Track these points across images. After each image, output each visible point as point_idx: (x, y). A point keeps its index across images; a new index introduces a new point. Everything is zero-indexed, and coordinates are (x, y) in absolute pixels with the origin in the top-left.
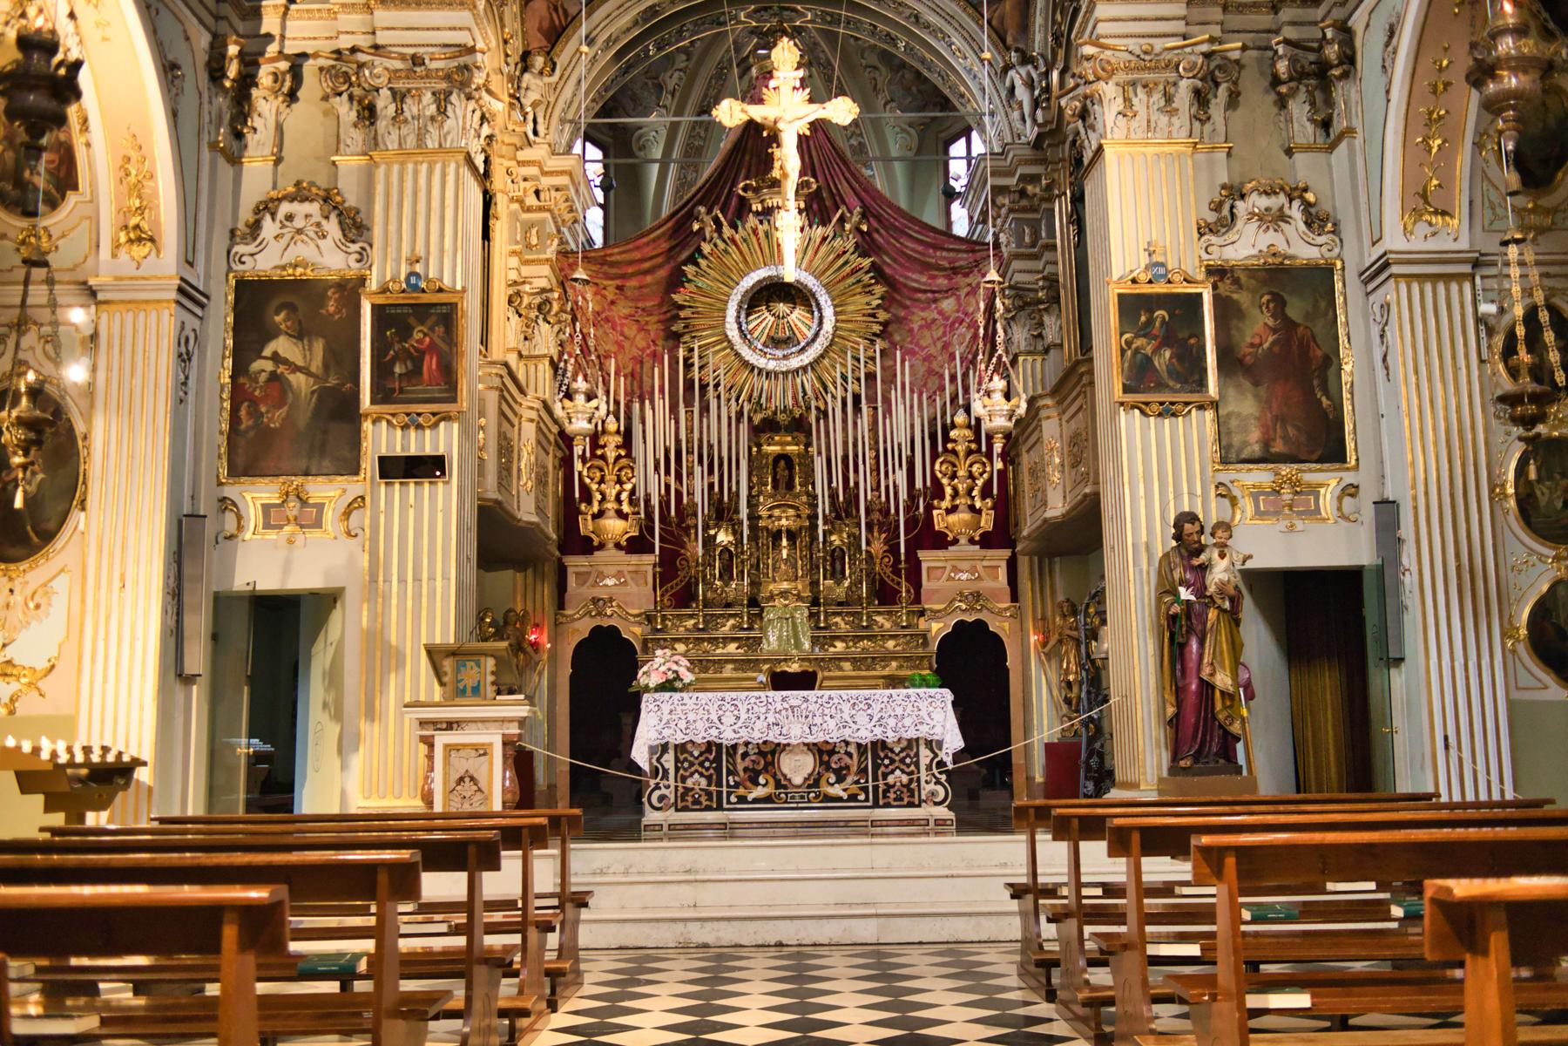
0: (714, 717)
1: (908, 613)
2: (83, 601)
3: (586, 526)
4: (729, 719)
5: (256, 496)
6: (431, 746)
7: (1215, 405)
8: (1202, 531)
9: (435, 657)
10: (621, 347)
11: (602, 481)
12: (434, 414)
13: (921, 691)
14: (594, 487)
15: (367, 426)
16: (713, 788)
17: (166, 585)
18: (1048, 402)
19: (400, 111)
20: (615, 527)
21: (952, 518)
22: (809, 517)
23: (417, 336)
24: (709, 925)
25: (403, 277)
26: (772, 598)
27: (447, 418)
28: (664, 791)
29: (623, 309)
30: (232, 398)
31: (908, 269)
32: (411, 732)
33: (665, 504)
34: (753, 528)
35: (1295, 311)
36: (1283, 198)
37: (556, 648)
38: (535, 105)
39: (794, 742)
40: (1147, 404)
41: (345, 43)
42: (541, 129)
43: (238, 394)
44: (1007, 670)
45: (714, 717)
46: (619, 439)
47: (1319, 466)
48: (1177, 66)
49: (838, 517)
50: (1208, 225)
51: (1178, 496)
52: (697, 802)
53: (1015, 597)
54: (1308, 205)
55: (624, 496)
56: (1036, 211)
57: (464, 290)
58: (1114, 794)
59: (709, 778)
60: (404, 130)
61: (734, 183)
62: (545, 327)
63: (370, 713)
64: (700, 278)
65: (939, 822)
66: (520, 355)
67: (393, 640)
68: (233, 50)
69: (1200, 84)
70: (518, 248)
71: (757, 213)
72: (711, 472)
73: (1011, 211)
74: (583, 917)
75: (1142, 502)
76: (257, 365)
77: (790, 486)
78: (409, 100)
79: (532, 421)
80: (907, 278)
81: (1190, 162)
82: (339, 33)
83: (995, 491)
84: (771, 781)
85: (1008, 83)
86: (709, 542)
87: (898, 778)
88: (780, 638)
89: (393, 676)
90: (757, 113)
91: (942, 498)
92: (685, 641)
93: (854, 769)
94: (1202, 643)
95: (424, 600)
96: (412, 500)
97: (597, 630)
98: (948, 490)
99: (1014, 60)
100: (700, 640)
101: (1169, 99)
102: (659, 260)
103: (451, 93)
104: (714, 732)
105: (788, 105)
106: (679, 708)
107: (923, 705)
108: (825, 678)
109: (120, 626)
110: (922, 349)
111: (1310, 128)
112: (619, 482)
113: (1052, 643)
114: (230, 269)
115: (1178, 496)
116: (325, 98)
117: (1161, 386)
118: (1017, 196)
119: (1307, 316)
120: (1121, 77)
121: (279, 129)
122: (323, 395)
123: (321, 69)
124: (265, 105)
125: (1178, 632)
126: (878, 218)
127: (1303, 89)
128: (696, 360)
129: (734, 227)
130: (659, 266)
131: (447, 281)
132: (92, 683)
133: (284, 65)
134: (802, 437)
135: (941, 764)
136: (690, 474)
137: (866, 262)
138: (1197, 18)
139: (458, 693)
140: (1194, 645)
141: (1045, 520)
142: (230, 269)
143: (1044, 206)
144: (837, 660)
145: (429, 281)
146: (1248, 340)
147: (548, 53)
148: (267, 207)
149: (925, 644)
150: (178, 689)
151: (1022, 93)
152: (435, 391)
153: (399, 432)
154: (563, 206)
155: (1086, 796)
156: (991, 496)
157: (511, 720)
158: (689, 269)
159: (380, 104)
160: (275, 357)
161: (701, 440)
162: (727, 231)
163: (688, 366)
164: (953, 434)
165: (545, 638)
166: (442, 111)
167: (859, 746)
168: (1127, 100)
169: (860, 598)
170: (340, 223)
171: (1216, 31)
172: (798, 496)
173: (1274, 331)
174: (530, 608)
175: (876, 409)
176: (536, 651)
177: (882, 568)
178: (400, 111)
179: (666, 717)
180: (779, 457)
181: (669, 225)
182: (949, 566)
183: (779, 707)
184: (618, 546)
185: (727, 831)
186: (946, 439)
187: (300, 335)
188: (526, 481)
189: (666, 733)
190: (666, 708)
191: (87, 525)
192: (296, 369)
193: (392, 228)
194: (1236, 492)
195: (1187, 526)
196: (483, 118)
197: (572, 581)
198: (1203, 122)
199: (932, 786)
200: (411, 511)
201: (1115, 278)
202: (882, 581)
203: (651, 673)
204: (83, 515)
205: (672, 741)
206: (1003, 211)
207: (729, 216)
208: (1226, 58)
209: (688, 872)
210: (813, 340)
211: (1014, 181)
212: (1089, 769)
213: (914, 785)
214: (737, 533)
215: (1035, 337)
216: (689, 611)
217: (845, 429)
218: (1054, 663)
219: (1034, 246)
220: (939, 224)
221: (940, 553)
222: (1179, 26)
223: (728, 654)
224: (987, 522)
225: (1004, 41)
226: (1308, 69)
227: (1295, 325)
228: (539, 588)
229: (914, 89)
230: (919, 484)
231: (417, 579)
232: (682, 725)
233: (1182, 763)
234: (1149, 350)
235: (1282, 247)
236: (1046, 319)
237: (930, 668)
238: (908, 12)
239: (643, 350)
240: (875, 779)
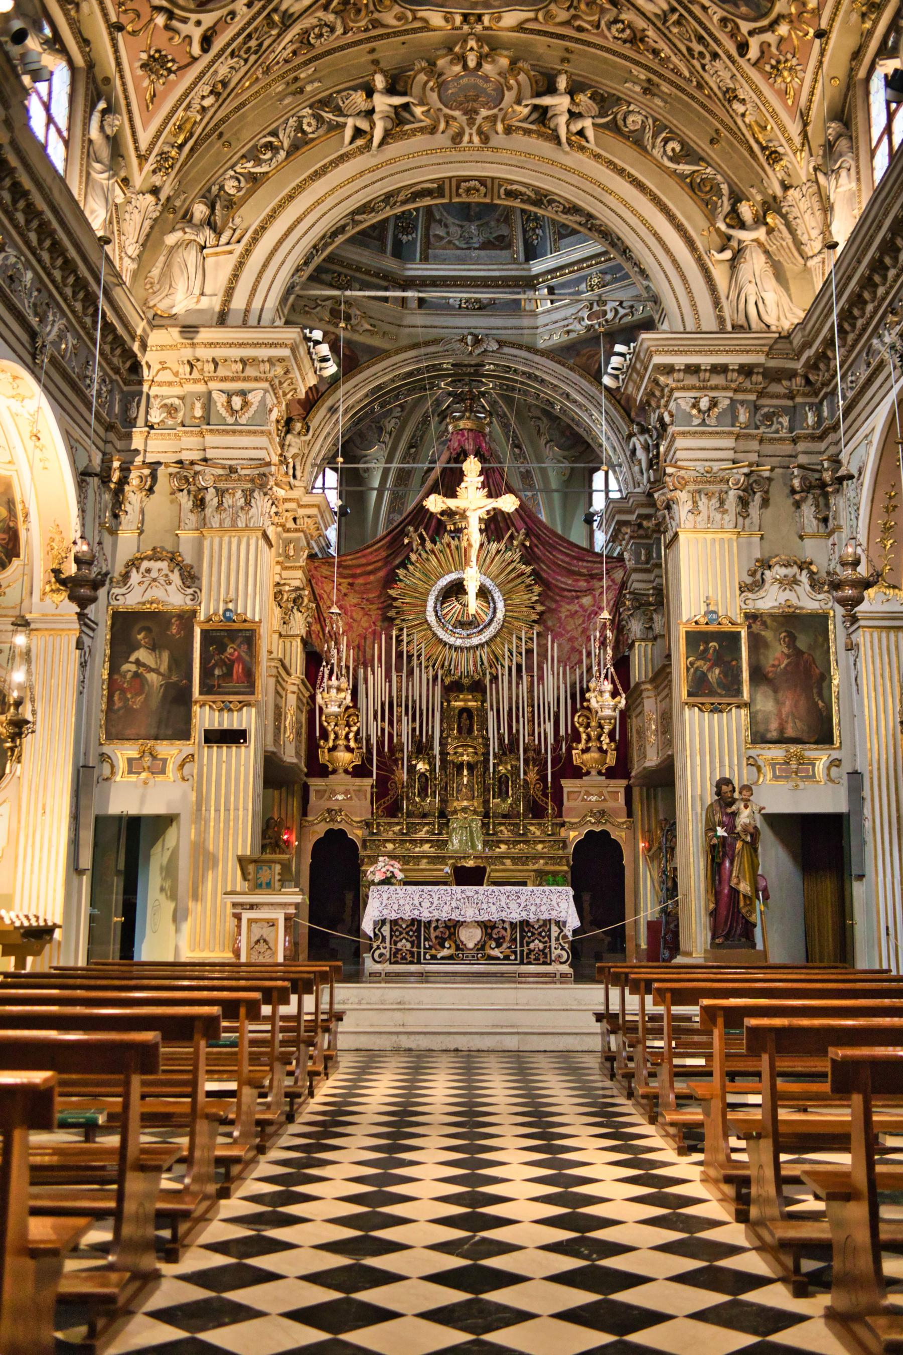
2: (19, 822)
3: (323, 757)
4: (426, 904)
5: (123, 753)
6: (240, 919)
7: (746, 705)
8: (734, 790)
9: (244, 864)
12: (240, 702)
13: (553, 888)
15: (196, 708)
16: (415, 949)
17: (71, 812)
18: (648, 686)
19: (220, 503)
20: (344, 757)
21: (586, 756)
22: (483, 754)
23: (230, 650)
24: (412, 1037)
25: (221, 612)
26: (455, 812)
27: (248, 704)
28: (382, 951)
29: (353, 599)
30: (109, 688)
31: (559, 574)
32: (230, 910)
33: (380, 743)
34: (443, 761)
35: (802, 643)
36: (795, 569)
37: (301, 845)
38: (294, 457)
39: (468, 920)
40: (703, 704)
41: (186, 456)
42: (298, 474)
43: (112, 686)
44: (622, 868)
47: (815, 746)
48: (728, 481)
49: (504, 754)
50: (746, 585)
51: (722, 765)
52: (404, 958)
53: (630, 814)
54: (812, 574)
55: (351, 735)
56: (649, 538)
57: (260, 621)
58: (679, 960)
59: (412, 943)
60: (224, 515)
62: (298, 615)
63: (196, 897)
64: (409, 577)
65: (563, 975)
66: (280, 635)
67: (211, 848)
68: (116, 464)
69: (741, 493)
70: (280, 559)
71: (451, 531)
72: (414, 720)
73: (631, 537)
74: (339, 1030)
75: (698, 768)
76: (125, 667)
77: (470, 731)
78: (227, 496)
80: (557, 580)
81: (735, 544)
82: (182, 449)
84: (453, 945)
85: (631, 446)
86: (412, 769)
87: (537, 945)
88: (460, 841)
89: (210, 872)
90: (452, 503)
91: (579, 741)
92: (393, 841)
93: (508, 939)
94: (732, 863)
95: (231, 823)
96: (224, 758)
97: (330, 832)
98: (584, 736)
99: (635, 430)
100: (403, 842)
101: (722, 502)
102: (380, 564)
103: (254, 491)
104: (416, 912)
105: (473, 500)
107: (554, 897)
108: (492, 871)
109: (42, 837)
111: (815, 522)
112: (348, 725)
113: (654, 849)
114: (109, 604)
115: (722, 765)
116: (173, 493)
117: (712, 693)
118: (636, 528)
119: (810, 647)
120: (691, 487)
121: (142, 512)
122: (168, 686)
123: (171, 474)
124: (133, 497)
125: (718, 854)
126: (538, 537)
127: (810, 496)
128: (405, 637)
129: (434, 542)
130: (379, 569)
131: (249, 615)
132: (24, 874)
133: (147, 472)
134: (479, 696)
135: (565, 937)
136: (399, 720)
137: (529, 569)
138: (742, 448)
139: (258, 886)
140: (727, 864)
141: (645, 768)
142: (109, 604)
143: (655, 536)
144: (501, 858)
145: (237, 615)
146: (771, 662)
147: (304, 419)
148: (134, 563)
150: (75, 877)
151: (641, 454)
152: (241, 687)
153: (217, 713)
154: (312, 527)
155: (664, 961)
157: (290, 904)
158: (401, 572)
159: (208, 498)
160: (138, 662)
161: (407, 697)
162: (429, 545)
163: (399, 642)
165: (294, 838)
166: (248, 503)
167: (511, 923)
168: (695, 502)
169: (519, 812)
170: (181, 575)
171: (754, 457)
172: (475, 739)
173: (788, 656)
174: (283, 816)
175: (532, 676)
176: (288, 847)
177: (535, 791)
178: (220, 503)
182: (583, 790)
184: (346, 771)
185: (424, 977)
187: (154, 648)
188: (289, 734)
189: (385, 912)
190: (385, 896)
191: (22, 773)
192: (150, 670)
193: (214, 579)
194: (761, 763)
195: (724, 788)
196: (273, 504)
198: (744, 518)
199: (559, 951)
200: (224, 765)
201: (684, 620)
202: (534, 800)
203: (376, 871)
204: (19, 766)
205: (389, 918)
206: (627, 537)
207: (430, 532)
208: (760, 476)
209: (399, 1003)
210: (489, 624)
211: (634, 517)
212: (666, 942)
213: (547, 950)
214: (431, 764)
216: (396, 820)
217: (510, 688)
218: (656, 863)
219: (647, 562)
220: (585, 544)
221: (577, 781)
222: (730, 454)
223: (423, 852)
224: (611, 759)
225: (629, 415)
226: (814, 483)
227: (803, 653)
228: (290, 800)
230: (562, 732)
231: (227, 810)
232: (396, 907)
233: (717, 941)
234: (705, 668)
235: (794, 601)
236: (655, 616)
237: (568, 865)
239: (366, 629)
240: (522, 945)
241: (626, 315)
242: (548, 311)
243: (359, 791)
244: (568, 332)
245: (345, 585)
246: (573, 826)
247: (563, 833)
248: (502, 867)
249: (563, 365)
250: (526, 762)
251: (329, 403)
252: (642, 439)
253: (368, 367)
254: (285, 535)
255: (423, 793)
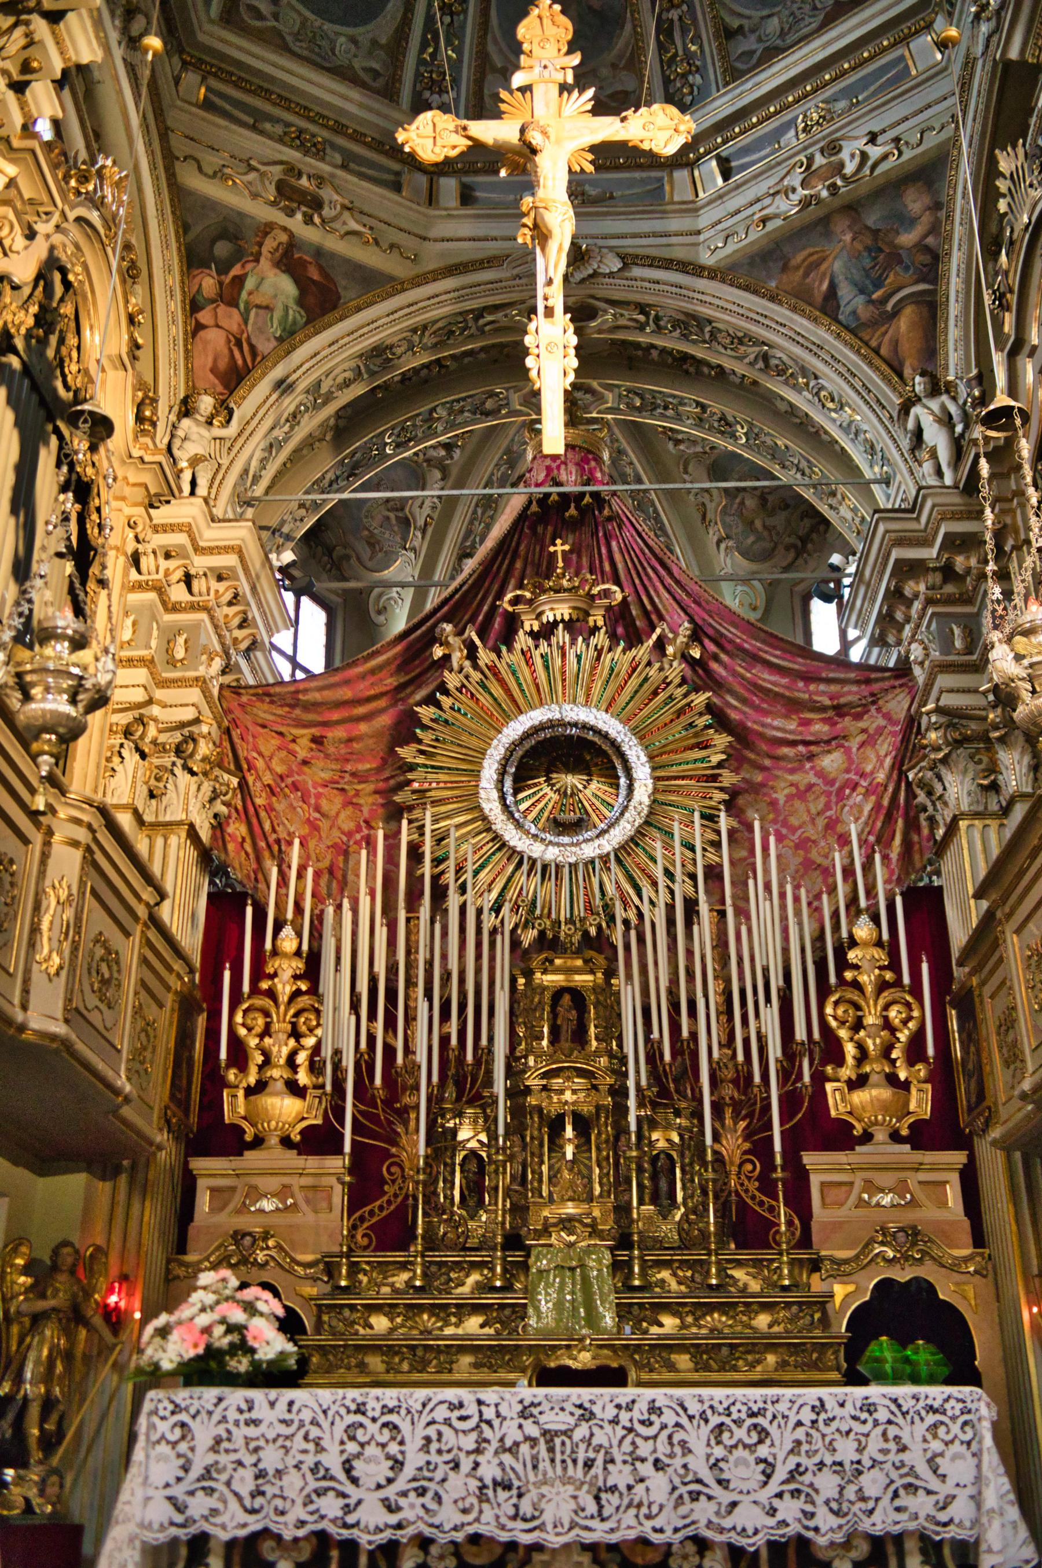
0: (333, 1461)
1: (792, 1263)
3: (234, 1107)
4: (372, 1469)
10: (314, 827)
11: (267, 1032)
13: (904, 1391)
14: (253, 1042)
20: (285, 1110)
21: (860, 1097)
26: (546, 1231)
31: (766, 713)
33: (364, 1068)
34: (518, 1111)
38: (195, 461)
39: (554, 1540)
45: (333, 1461)
46: (299, 965)
49: (664, 1092)
53: (979, 1239)
55: (302, 1058)
61: (500, 596)
62: (183, 778)
72: (445, 1016)
73: (929, 602)
77: (580, 1037)
79: (75, 844)
83: (931, 1051)
85: (911, 425)
86: (442, 1141)
88: (559, 1305)
92: (389, 1310)
98: (850, 1050)
102: (382, 703)
106: (239, 1434)
107: (913, 1433)
110: (793, 830)
112: (295, 1033)
118: (938, 577)
134: (600, 960)
136: (410, 1018)
144: (665, 1348)
149: (825, 1322)
151: (935, 437)
156: (922, 1057)
161: (429, 963)
162: (485, 657)
164: (852, 956)
169: (704, 1234)
177: (743, 1181)
179: (201, 1460)
180: (559, 993)
181: (399, 648)
182: (858, 1179)
183: (513, 1434)
184: (286, 1142)
186: (842, 964)
190: (204, 1433)
197: (204, 1202)
202: (742, 1204)
211: (934, 552)
215: (985, 788)
216: (399, 1257)
221: (841, 1157)
224: (920, 1103)
229: (758, 524)
230: (800, 1033)
238: (753, 351)
239: (349, 834)
241: (885, 157)
242: (720, 197)
243: (314, 1188)
244: (764, 221)
245: (305, 742)
246: (841, 1270)
247: (817, 1284)
248: (668, 1376)
249: (755, 292)
250: (717, 1109)
251: (278, 372)
252: (934, 405)
253: (359, 309)
254: (169, 618)
255: (475, 1193)
